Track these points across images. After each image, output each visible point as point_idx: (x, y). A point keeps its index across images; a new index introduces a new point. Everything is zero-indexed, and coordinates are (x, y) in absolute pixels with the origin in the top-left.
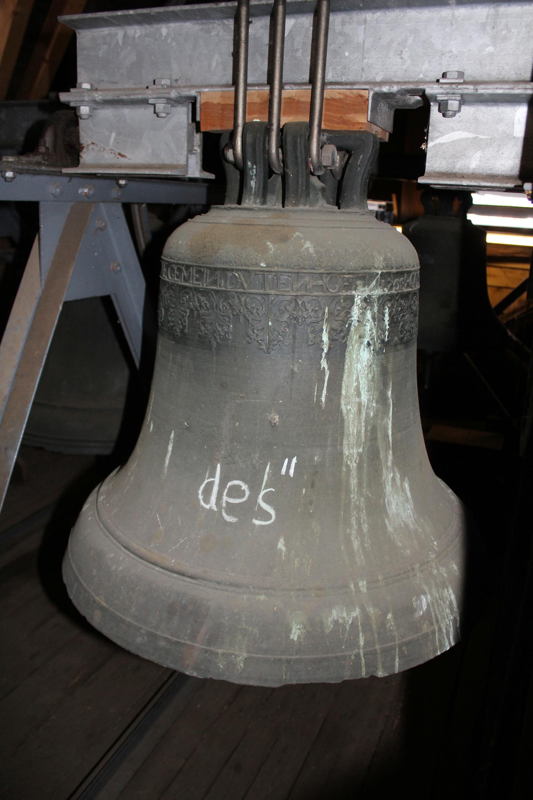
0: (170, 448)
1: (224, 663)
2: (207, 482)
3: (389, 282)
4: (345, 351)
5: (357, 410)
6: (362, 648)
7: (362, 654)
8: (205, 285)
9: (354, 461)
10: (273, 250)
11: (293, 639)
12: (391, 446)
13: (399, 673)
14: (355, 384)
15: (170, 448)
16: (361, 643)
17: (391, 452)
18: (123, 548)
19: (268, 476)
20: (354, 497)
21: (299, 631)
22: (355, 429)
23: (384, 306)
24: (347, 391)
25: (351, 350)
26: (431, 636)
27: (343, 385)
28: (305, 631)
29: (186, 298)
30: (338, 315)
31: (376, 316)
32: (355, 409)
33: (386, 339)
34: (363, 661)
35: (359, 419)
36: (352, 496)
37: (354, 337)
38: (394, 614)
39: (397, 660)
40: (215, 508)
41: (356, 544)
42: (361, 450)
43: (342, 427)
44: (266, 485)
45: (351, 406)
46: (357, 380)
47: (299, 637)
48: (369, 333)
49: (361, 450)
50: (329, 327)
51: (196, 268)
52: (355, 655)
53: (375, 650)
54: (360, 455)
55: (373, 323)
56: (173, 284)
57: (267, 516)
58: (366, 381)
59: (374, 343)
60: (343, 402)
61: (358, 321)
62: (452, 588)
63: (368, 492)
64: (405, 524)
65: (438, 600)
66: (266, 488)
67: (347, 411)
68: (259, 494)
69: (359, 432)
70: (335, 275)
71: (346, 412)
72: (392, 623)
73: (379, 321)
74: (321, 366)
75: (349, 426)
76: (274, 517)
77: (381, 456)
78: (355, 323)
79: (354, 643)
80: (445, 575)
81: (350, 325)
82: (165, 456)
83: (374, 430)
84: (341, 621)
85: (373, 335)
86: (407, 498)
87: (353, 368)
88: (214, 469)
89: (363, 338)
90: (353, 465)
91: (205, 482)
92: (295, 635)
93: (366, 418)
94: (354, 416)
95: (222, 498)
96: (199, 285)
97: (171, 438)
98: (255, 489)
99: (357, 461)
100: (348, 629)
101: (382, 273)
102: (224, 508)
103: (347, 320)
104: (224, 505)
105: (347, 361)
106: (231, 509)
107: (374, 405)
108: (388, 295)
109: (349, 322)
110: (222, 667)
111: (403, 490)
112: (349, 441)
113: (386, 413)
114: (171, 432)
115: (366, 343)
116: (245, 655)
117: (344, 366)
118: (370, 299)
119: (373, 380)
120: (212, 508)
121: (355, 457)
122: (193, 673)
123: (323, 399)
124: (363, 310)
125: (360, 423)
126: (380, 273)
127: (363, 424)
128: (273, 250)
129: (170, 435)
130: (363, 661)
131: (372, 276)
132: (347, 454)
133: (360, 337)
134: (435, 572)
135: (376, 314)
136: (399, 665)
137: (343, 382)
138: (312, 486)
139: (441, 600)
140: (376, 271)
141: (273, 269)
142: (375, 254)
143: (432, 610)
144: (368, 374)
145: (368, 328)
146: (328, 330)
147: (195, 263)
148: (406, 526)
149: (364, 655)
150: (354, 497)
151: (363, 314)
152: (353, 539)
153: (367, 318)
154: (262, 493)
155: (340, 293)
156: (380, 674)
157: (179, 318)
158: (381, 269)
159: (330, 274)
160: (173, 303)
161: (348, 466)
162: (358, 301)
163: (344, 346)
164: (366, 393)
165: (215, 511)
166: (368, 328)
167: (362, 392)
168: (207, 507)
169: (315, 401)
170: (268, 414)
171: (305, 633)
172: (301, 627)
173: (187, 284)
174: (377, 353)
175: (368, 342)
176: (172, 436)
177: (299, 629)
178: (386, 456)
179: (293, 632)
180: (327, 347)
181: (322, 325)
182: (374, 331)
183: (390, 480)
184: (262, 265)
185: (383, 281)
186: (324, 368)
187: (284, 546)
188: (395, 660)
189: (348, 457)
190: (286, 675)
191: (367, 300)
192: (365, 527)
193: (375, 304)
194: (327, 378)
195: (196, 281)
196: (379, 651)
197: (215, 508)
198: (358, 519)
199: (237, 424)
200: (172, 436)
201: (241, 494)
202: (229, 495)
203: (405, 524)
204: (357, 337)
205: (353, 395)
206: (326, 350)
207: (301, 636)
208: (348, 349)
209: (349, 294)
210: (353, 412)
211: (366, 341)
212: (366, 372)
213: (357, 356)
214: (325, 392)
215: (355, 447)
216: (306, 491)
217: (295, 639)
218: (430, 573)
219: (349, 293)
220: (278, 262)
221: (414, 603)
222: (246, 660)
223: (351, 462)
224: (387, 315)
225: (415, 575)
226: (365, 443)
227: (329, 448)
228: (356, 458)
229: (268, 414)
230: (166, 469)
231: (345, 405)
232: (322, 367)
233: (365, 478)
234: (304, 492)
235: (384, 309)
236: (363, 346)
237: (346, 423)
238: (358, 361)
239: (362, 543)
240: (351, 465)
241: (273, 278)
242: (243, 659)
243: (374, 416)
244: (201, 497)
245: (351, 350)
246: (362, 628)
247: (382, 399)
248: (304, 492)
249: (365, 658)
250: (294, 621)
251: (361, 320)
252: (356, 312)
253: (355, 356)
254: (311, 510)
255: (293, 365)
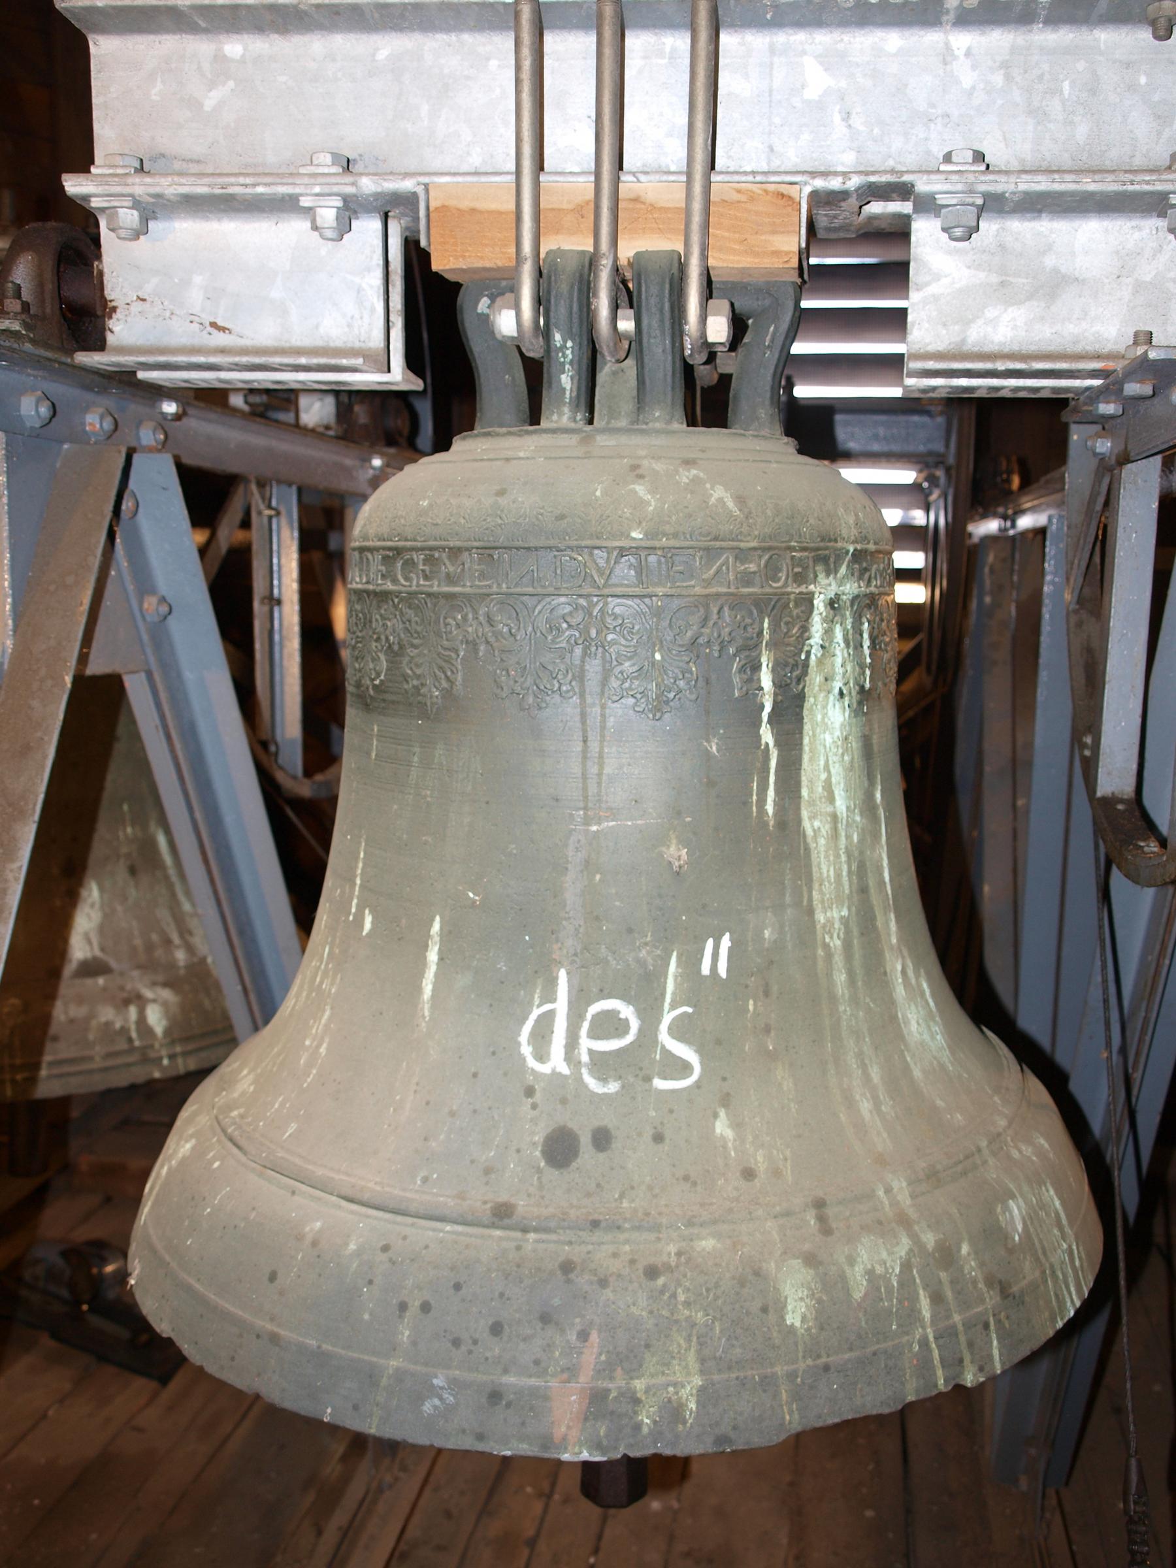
0: (433, 956)
1: (651, 1409)
2: (539, 1016)
3: (866, 570)
4: (802, 707)
5: (831, 828)
6: (929, 1323)
7: (931, 1337)
8: (504, 586)
9: (835, 936)
10: (653, 503)
11: (793, 1324)
12: (891, 902)
13: (1004, 1372)
14: (824, 776)
15: (433, 956)
16: (924, 1312)
17: (892, 916)
18: (344, 1203)
19: (675, 980)
20: (845, 1010)
21: (803, 1304)
22: (832, 869)
23: (860, 617)
24: (811, 791)
25: (812, 706)
26: (1042, 1287)
27: (803, 778)
28: (813, 1302)
29: (455, 619)
30: (787, 633)
31: (850, 637)
32: (828, 827)
33: (867, 685)
34: (936, 1354)
35: (837, 848)
36: (841, 1008)
37: (815, 678)
38: (972, 1243)
39: (995, 1343)
40: (564, 1069)
41: (865, 1106)
42: (845, 912)
43: (808, 866)
44: (673, 1001)
45: (821, 821)
46: (827, 768)
47: (804, 1319)
48: (841, 671)
49: (845, 912)
50: (772, 658)
51: (480, 551)
52: (919, 1341)
53: (954, 1326)
54: (845, 922)
55: (845, 651)
56: (412, 595)
57: (684, 1068)
58: (841, 769)
59: (850, 693)
60: (805, 814)
61: (822, 647)
62: (1053, 1185)
63: (868, 1000)
64: (939, 1062)
65: (1037, 1208)
66: (673, 1007)
67: (814, 831)
68: (659, 1022)
69: (838, 876)
70: (776, 552)
71: (812, 834)
72: (973, 1263)
73: (855, 648)
74: (761, 739)
75: (819, 864)
76: (697, 1069)
77: (879, 924)
78: (816, 652)
79: (911, 1315)
80: (1034, 1158)
81: (808, 653)
82: (421, 974)
83: (862, 867)
84: (879, 1270)
85: (848, 674)
86: (931, 1011)
87: (818, 742)
88: (552, 982)
89: (833, 680)
90: (836, 943)
91: (533, 1017)
92: (794, 1317)
93: (846, 848)
94: (827, 843)
95: (578, 1044)
96: (490, 587)
97: (432, 933)
98: (650, 1014)
99: (842, 935)
100: (895, 1284)
101: (855, 550)
102: (586, 1065)
103: (803, 645)
104: (585, 1058)
105: (807, 728)
106: (602, 1064)
107: (858, 818)
108: (866, 595)
109: (806, 648)
110: (648, 1421)
111: (922, 994)
112: (821, 893)
113: (876, 836)
114: (433, 920)
115: (836, 691)
116: (698, 1381)
117: (801, 739)
118: (838, 603)
119: (851, 768)
120: (558, 1070)
121: (837, 925)
122: (581, 1453)
123: (770, 808)
124: (829, 621)
125: (838, 856)
126: (852, 550)
127: (844, 858)
128: (653, 503)
129: (431, 925)
130: (936, 1354)
131: (839, 556)
132: (822, 921)
133: (826, 680)
134: (1015, 1154)
135: (851, 632)
136: (1001, 1355)
137: (803, 773)
138: (767, 994)
139: (1041, 1209)
140: (845, 545)
141: (657, 544)
142: (841, 511)
143: (1032, 1230)
144: (843, 755)
145: (839, 660)
146: (770, 665)
147: (475, 540)
148: (942, 1067)
149: (936, 1338)
150: (845, 1010)
151: (828, 632)
152: (858, 1097)
153: (835, 641)
154: (667, 1019)
155: (789, 589)
156: (970, 1378)
157: (437, 664)
158: (853, 542)
159: (770, 548)
160: (416, 635)
161: (826, 946)
162: (819, 603)
163: (801, 698)
164: (842, 793)
165: (565, 1076)
166: (839, 660)
167: (836, 793)
168: (545, 1069)
169: (755, 814)
170: (664, 849)
171: (814, 1306)
172: (805, 1293)
173: (457, 589)
174: (857, 712)
175: (841, 690)
176: (436, 927)
177: (802, 1299)
178: (887, 923)
179: (790, 1308)
180: (771, 699)
181: (759, 655)
182: (849, 668)
183: (899, 975)
184: (634, 534)
185: (856, 566)
186: (767, 744)
187: (728, 1127)
188: (992, 1343)
189: (824, 927)
190: (791, 1413)
191: (832, 604)
192: (875, 1074)
193: (848, 613)
194: (773, 764)
195: (479, 580)
196: (960, 1328)
197: (564, 1069)
198: (860, 1055)
199: (598, 877)
200: (436, 927)
201: (621, 1028)
202: (594, 1035)
203: (939, 1062)
204: (823, 680)
205: (821, 798)
206: (768, 707)
207: (809, 1315)
208: (807, 705)
209: (805, 590)
210: (825, 833)
211: (837, 684)
212: (840, 751)
213: (823, 718)
214: (771, 794)
215: (834, 906)
216: (755, 1004)
217: (798, 1324)
218: (1009, 1157)
219: (803, 589)
220: (667, 528)
221: (1000, 1218)
222: (703, 1393)
223: (831, 938)
224: (866, 636)
225: (985, 1162)
226: (850, 897)
227: (789, 911)
228: (840, 929)
229: (664, 849)
230: (427, 1006)
231: (810, 818)
232: (763, 742)
233: (859, 971)
234: (751, 1008)
235: (862, 624)
236: (831, 698)
237: (814, 855)
238: (826, 728)
239: (877, 1104)
240: (832, 945)
241: (659, 562)
242: (694, 1391)
243: (859, 842)
244: (526, 1050)
245: (812, 706)
246: (921, 1281)
247: (869, 807)
248: (751, 1008)
249: (938, 1347)
250: (789, 1281)
251: (827, 644)
252: (817, 626)
253: (819, 717)
254: (769, 1044)
255: (708, 741)
